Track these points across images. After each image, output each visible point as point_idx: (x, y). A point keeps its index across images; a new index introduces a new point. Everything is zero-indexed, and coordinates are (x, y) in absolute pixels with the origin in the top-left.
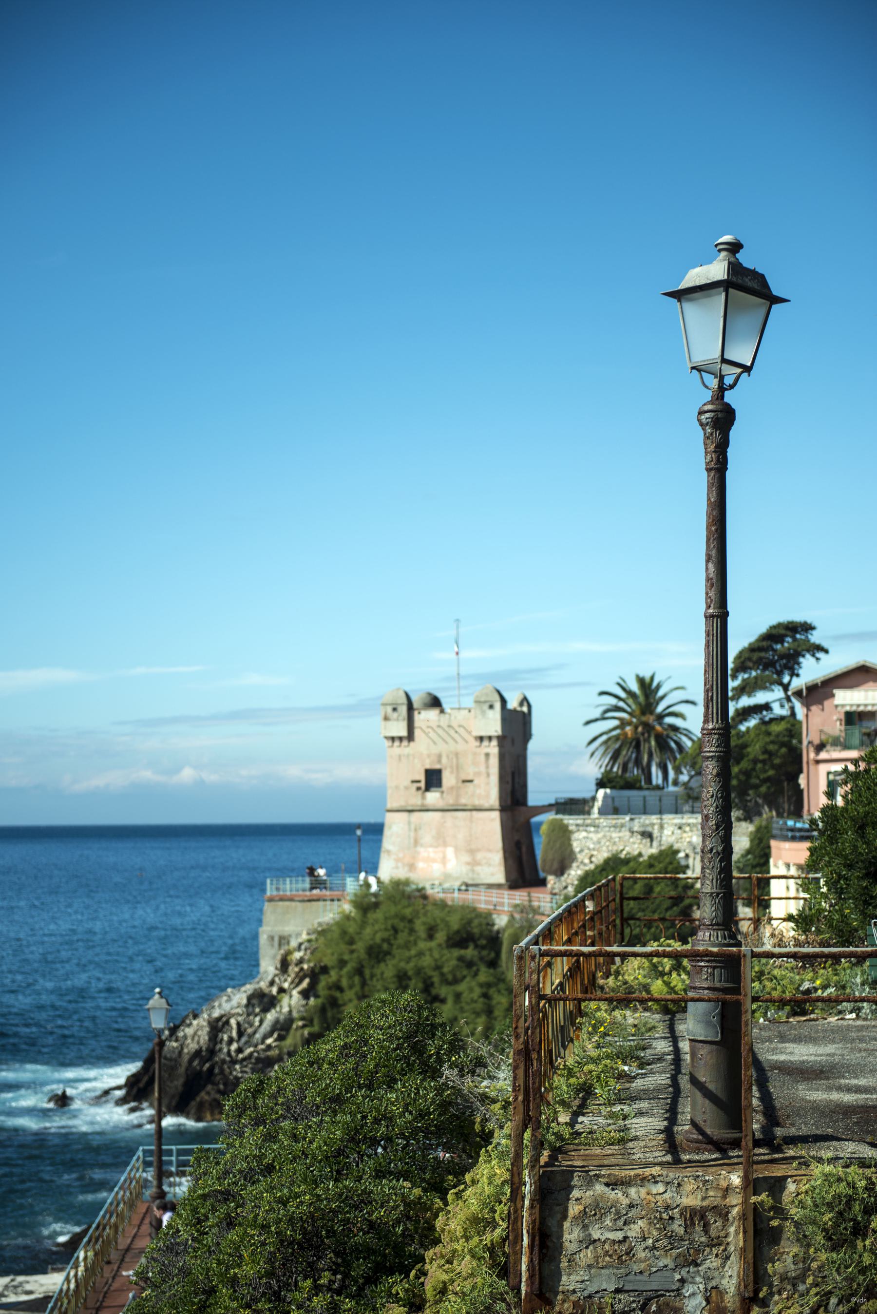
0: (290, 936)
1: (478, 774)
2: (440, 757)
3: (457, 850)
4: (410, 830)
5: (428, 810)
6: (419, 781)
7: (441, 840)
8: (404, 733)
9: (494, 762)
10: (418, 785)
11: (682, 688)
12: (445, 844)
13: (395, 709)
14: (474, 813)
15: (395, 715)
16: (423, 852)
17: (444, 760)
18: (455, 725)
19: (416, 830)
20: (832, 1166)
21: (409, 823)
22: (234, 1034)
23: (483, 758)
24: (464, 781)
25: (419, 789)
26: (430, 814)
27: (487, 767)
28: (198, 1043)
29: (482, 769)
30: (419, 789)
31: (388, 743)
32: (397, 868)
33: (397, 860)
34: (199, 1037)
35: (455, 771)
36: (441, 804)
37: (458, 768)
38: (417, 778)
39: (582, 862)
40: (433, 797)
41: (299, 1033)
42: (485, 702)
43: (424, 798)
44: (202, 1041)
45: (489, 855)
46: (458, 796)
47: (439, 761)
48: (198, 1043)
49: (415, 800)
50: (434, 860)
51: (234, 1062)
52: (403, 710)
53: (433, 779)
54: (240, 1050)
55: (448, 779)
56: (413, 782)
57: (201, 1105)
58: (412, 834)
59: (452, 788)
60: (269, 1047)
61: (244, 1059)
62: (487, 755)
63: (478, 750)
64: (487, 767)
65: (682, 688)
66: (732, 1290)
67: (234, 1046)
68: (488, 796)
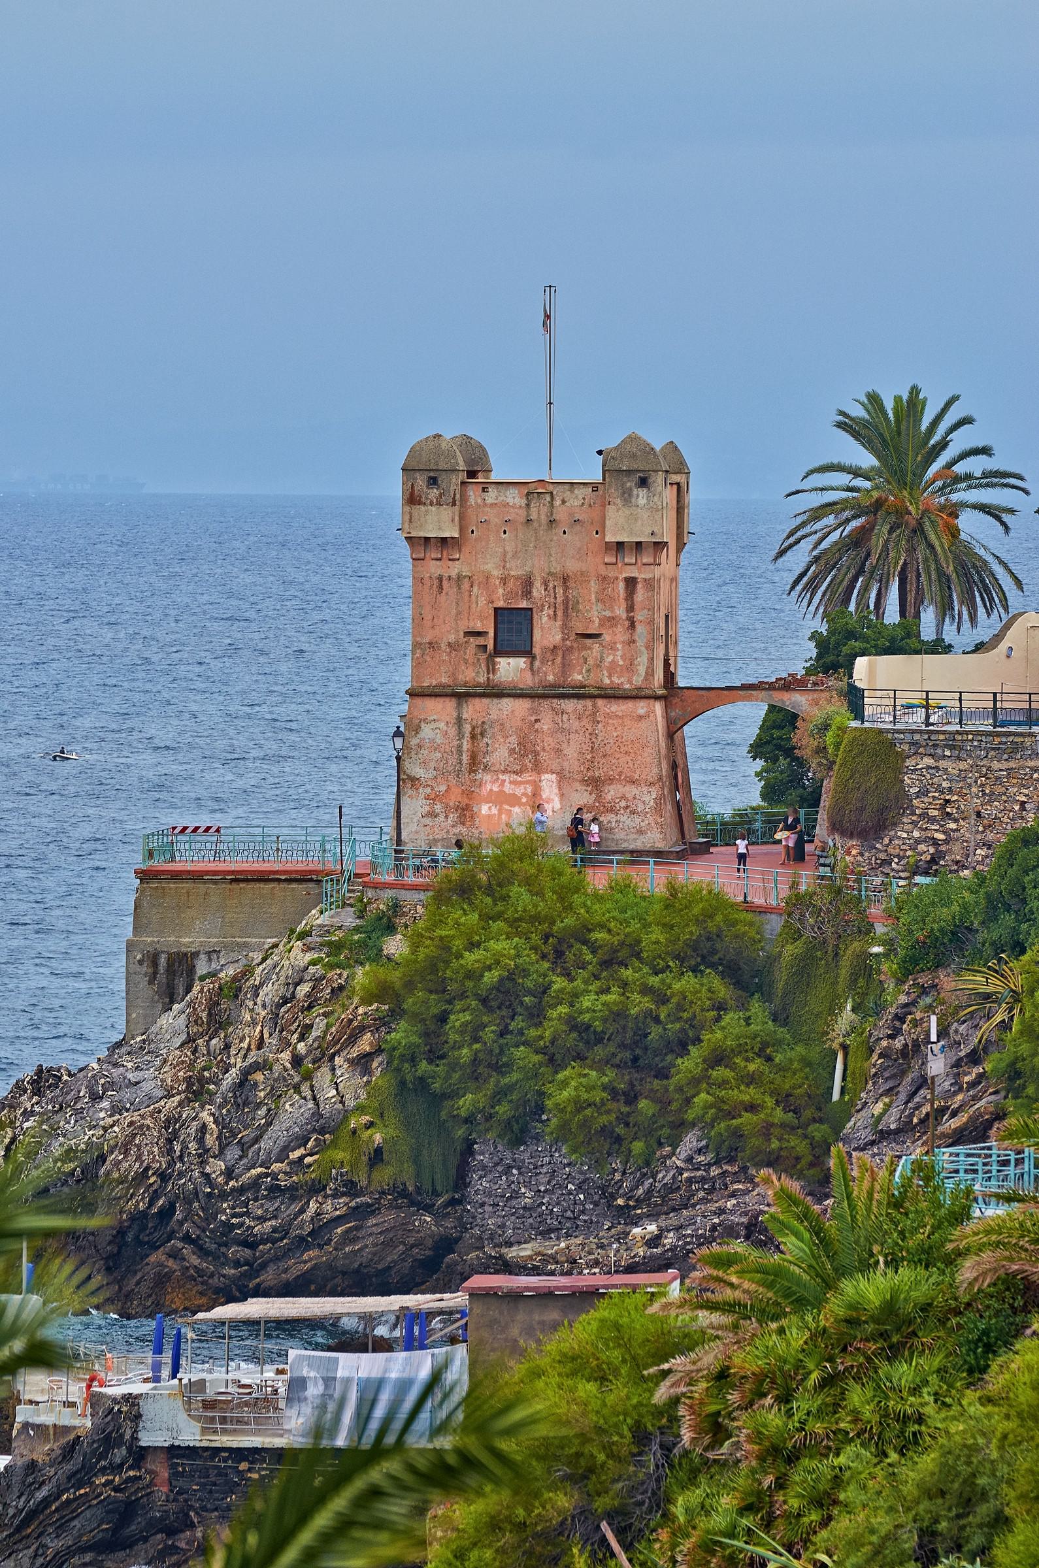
0: (196, 955)
1: (612, 621)
2: (528, 583)
3: (563, 777)
5: (500, 695)
6: (479, 634)
7: (528, 756)
10: (481, 641)
11: (985, 451)
12: (538, 768)
13: (433, 481)
15: (434, 493)
16: (489, 784)
17: (538, 591)
19: (473, 737)
21: (459, 721)
26: (507, 703)
27: (630, 608)
29: (620, 611)
32: (433, 815)
33: (433, 798)
34: (139, 1147)
35: (560, 613)
36: (528, 681)
37: (568, 608)
38: (479, 627)
39: (924, 815)
42: (629, 472)
43: (492, 668)
45: (631, 791)
46: (566, 667)
50: (514, 800)
54: (229, 1174)
56: (468, 634)
57: (162, 1280)
61: (242, 1190)
63: (612, 572)
64: (630, 608)
65: (985, 451)
67: (216, 1167)
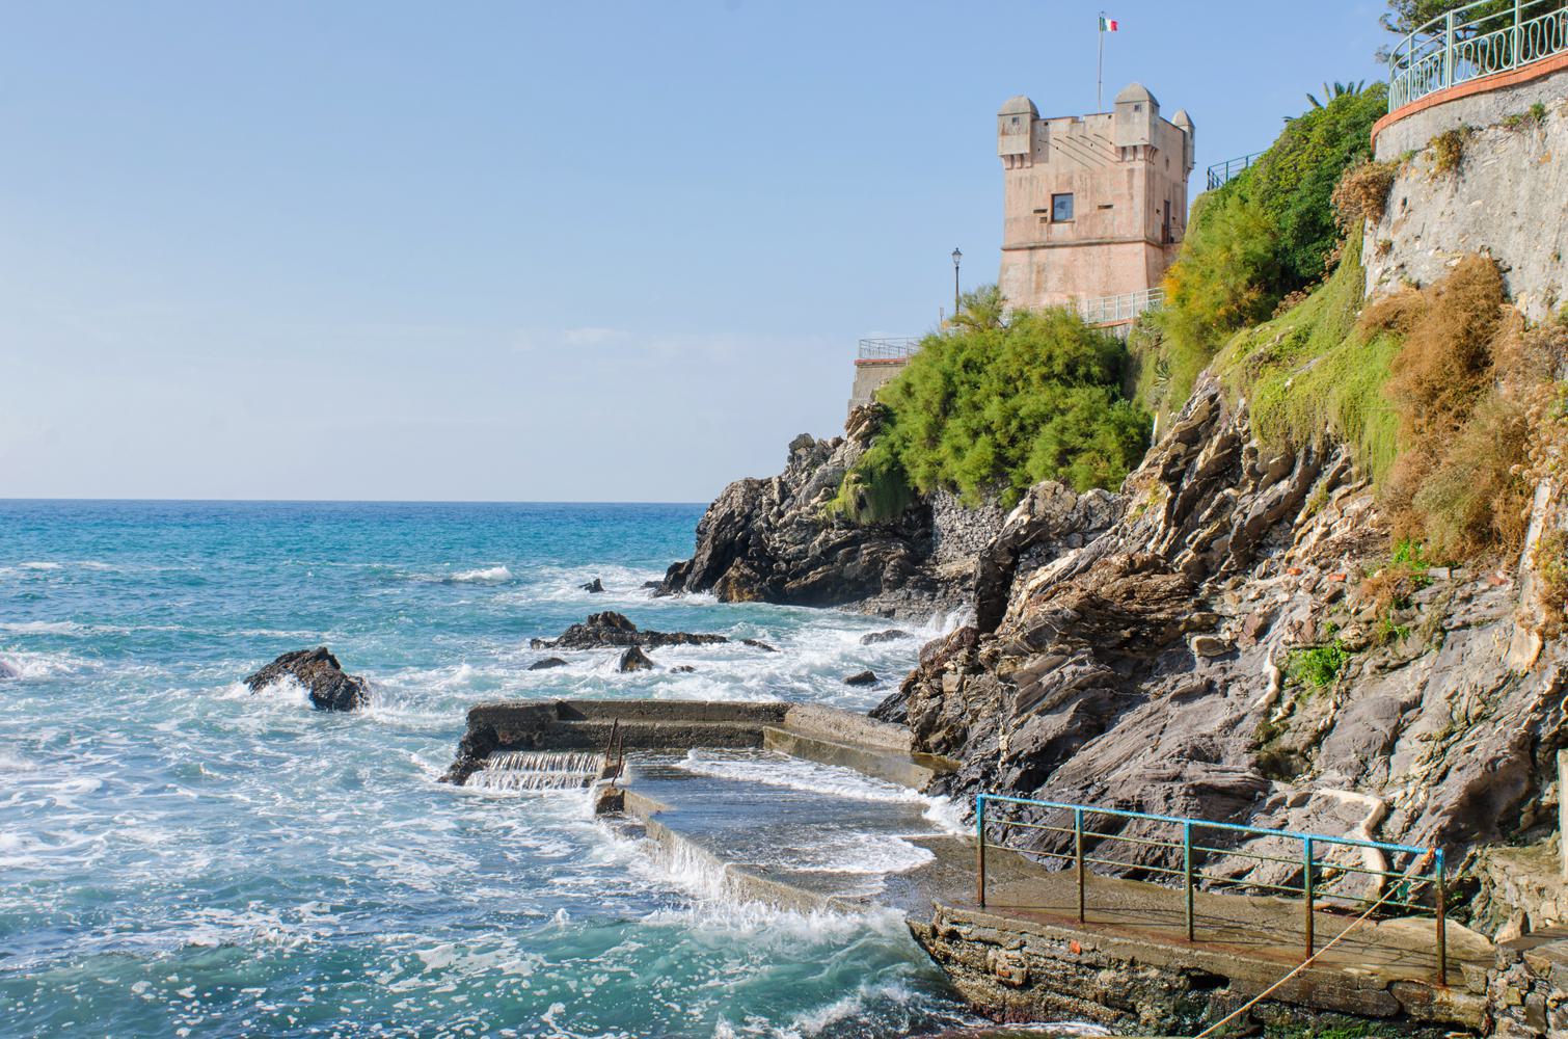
1: (1120, 196)
4: (1031, 272)
5: (1053, 247)
6: (1044, 211)
8: (1026, 150)
9: (1140, 182)
14: (1112, 247)
17: (1076, 184)
18: (1089, 135)
20: (274, 915)
21: (1030, 264)
22: (776, 496)
23: (1125, 174)
24: (1100, 207)
25: (1044, 220)
27: (1131, 187)
28: (730, 505)
29: (1124, 189)
30: (1044, 220)
31: (1005, 164)
36: (1070, 237)
37: (1095, 189)
40: (1060, 231)
41: (851, 487)
43: (1049, 231)
44: (735, 505)
47: (1070, 182)
48: (730, 505)
49: (1037, 235)
51: (771, 529)
52: (1026, 120)
53: (1059, 206)
55: (1081, 207)
58: (1034, 277)
59: (1085, 217)
60: (815, 508)
61: (785, 525)
62: (1131, 171)
64: (1131, 187)
66: (556, 595)
68: (1131, 223)
